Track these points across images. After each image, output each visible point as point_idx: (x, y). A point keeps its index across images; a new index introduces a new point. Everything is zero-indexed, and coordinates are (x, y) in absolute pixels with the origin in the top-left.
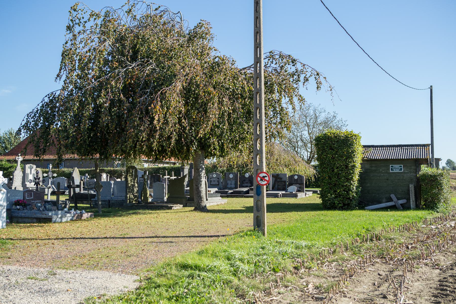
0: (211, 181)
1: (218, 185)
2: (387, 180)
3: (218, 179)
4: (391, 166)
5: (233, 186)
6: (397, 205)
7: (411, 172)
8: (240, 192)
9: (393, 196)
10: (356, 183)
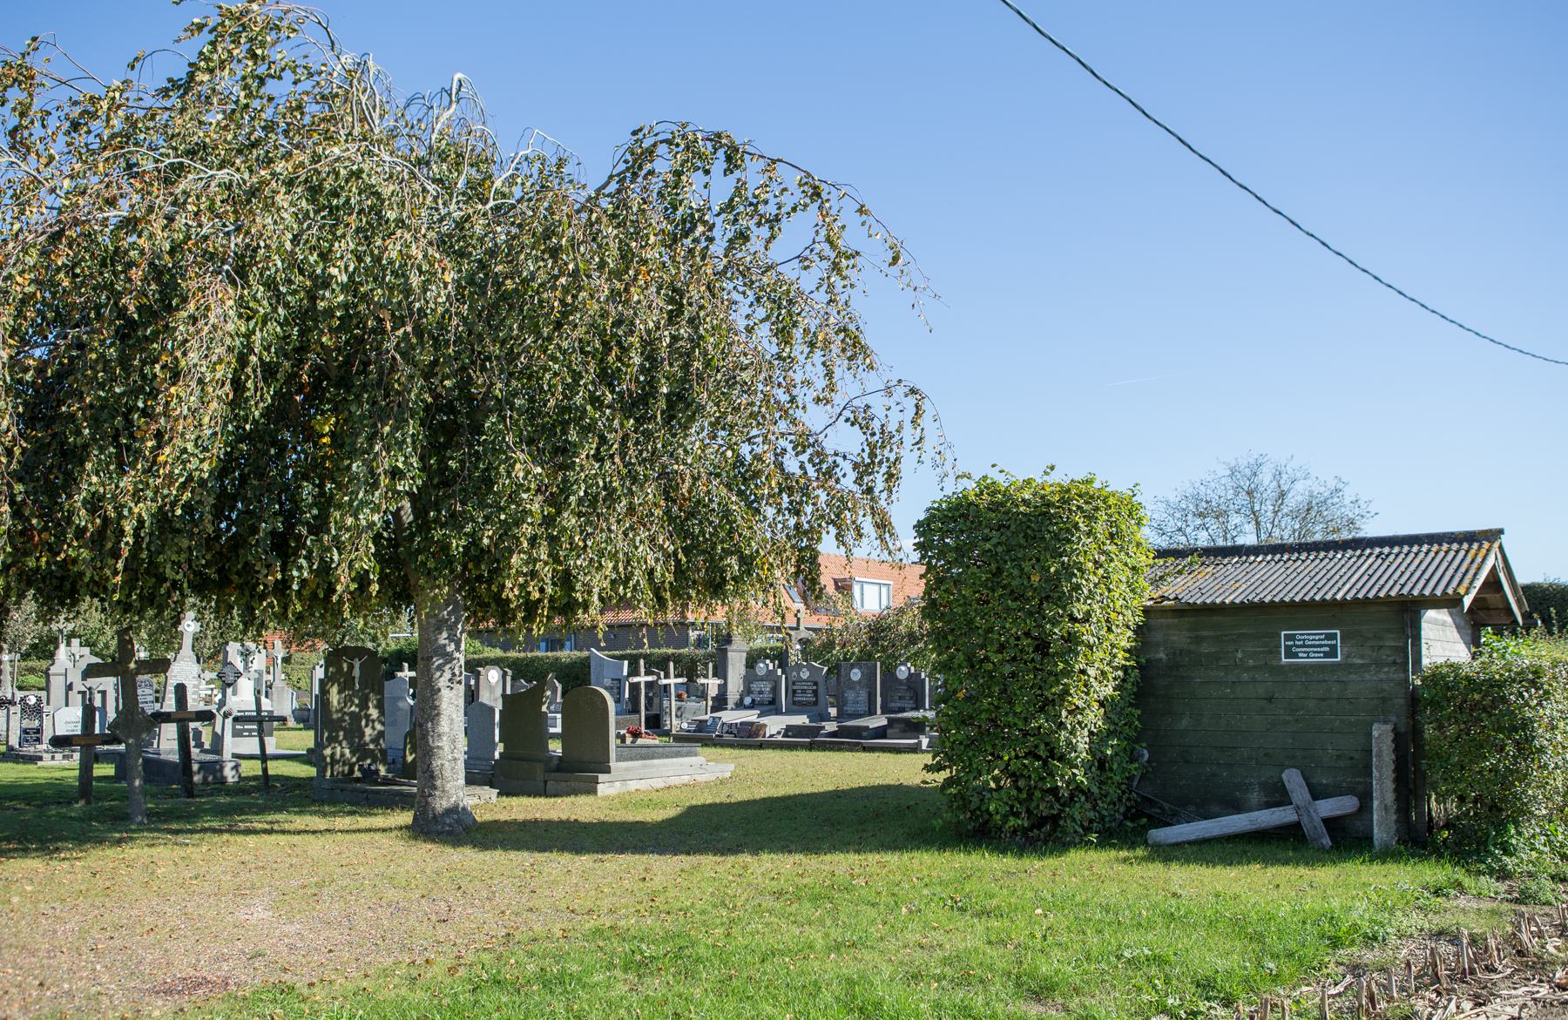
0: (794, 692)
1: (816, 703)
2: (1270, 699)
3: (816, 684)
4: (1288, 638)
5: (863, 708)
6: (1305, 821)
7: (1379, 664)
8: (858, 732)
9: (1293, 779)
10: (1094, 718)
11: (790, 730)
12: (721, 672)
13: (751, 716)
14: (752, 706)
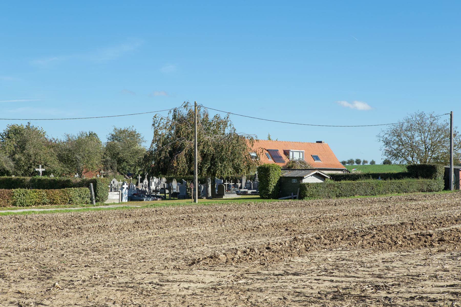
11: (252, 192)
12: (241, 182)
13: (246, 190)
14: (246, 188)
